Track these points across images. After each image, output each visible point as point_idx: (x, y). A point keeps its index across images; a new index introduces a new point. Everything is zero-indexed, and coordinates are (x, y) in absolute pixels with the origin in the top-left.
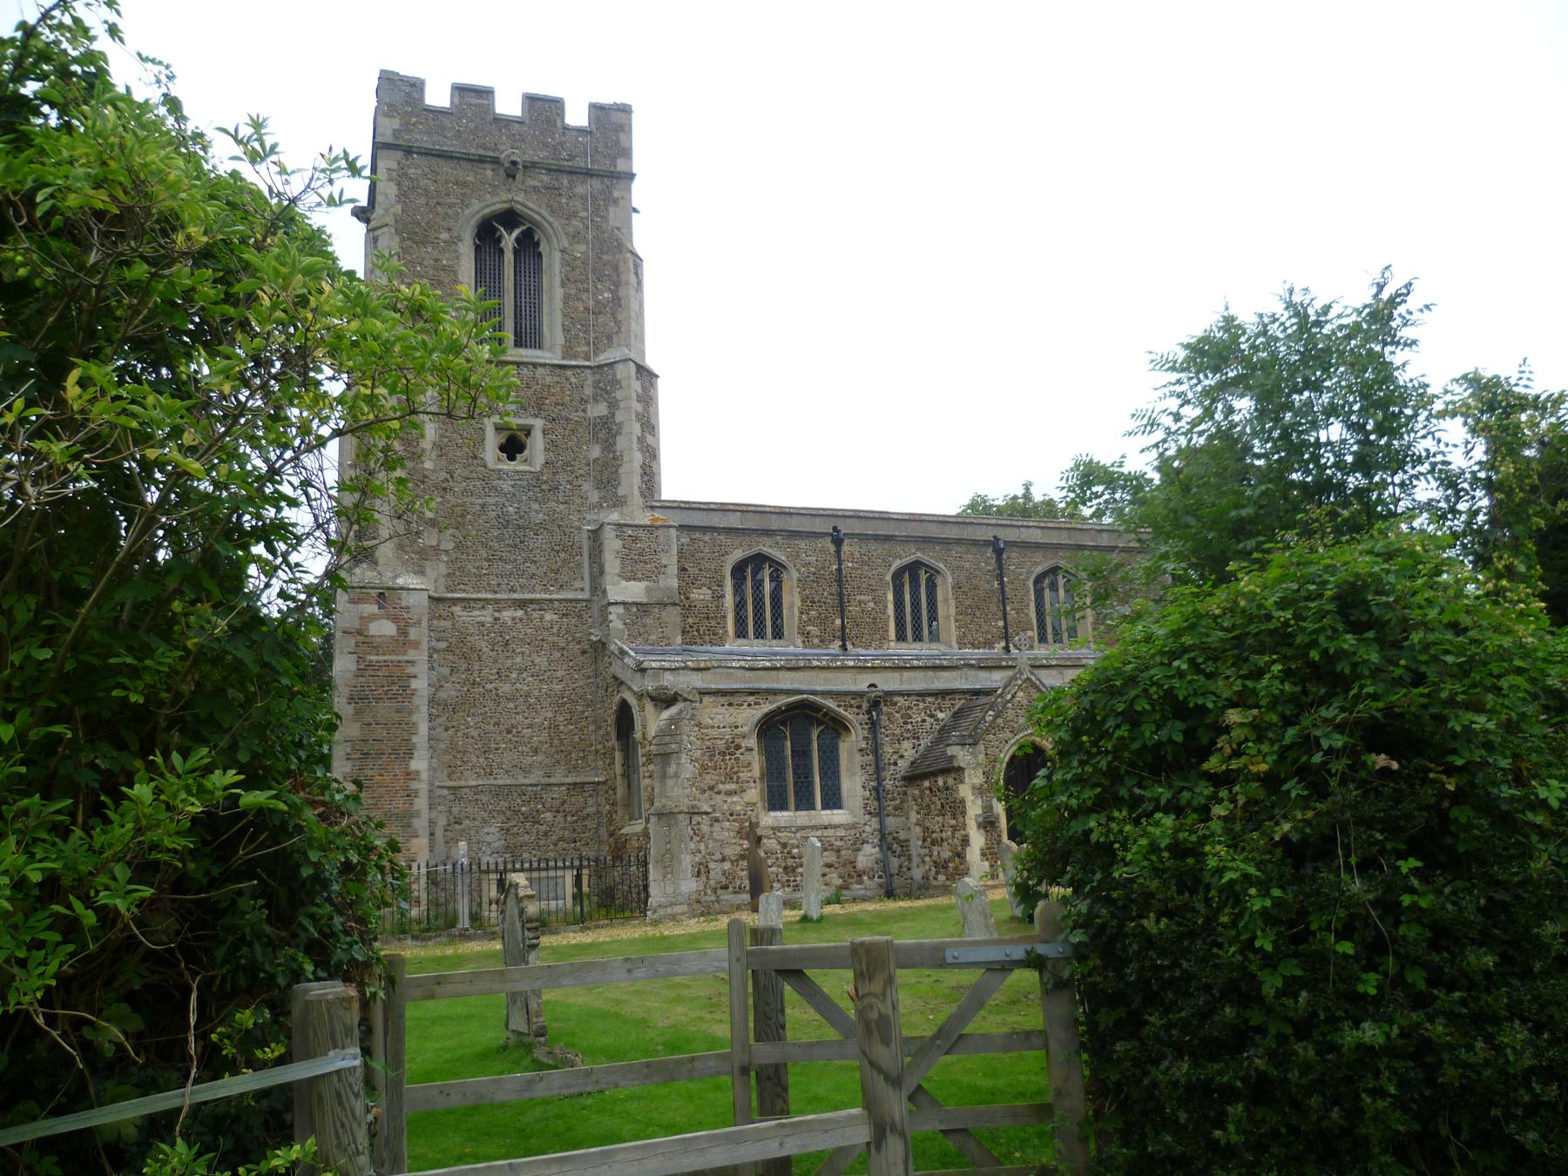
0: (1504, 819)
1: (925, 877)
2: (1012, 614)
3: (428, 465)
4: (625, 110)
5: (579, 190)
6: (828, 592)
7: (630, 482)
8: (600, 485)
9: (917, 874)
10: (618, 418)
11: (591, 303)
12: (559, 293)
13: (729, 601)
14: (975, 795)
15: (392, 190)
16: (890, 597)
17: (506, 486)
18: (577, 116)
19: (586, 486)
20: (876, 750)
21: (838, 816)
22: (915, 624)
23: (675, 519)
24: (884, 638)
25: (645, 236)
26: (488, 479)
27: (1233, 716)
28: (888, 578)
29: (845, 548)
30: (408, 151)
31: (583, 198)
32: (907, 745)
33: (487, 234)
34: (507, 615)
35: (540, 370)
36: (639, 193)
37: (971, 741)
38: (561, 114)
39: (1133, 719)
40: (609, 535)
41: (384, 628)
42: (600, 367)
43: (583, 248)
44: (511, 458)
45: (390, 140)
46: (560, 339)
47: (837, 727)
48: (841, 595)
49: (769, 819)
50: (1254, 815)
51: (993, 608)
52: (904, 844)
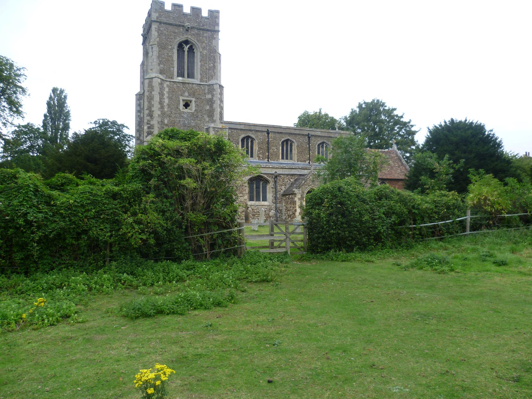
0: (350, 212)
1: (286, 219)
2: (311, 154)
3: (166, 110)
4: (218, 12)
5: (205, 35)
6: (265, 146)
7: (217, 116)
8: (209, 116)
9: (284, 218)
10: (214, 99)
11: (208, 67)
12: (199, 64)
14: (299, 201)
16: (281, 148)
17: (185, 116)
18: (205, 14)
19: (205, 116)
20: (276, 188)
21: (266, 203)
22: (286, 155)
23: (228, 126)
24: (279, 158)
25: (222, 49)
26: (181, 113)
27: (326, 200)
28: (280, 143)
29: (270, 135)
30: (160, 23)
31: (206, 37)
32: (283, 187)
33: (180, 46)
35: (194, 85)
36: (221, 35)
37: (299, 187)
38: (201, 13)
39: (316, 199)
40: (211, 130)
42: (210, 85)
43: (206, 51)
44: (186, 108)
45: (156, 20)
46: (199, 77)
47: (266, 182)
48: (268, 147)
49: (250, 203)
50: (327, 210)
51: (307, 152)
52: (281, 210)
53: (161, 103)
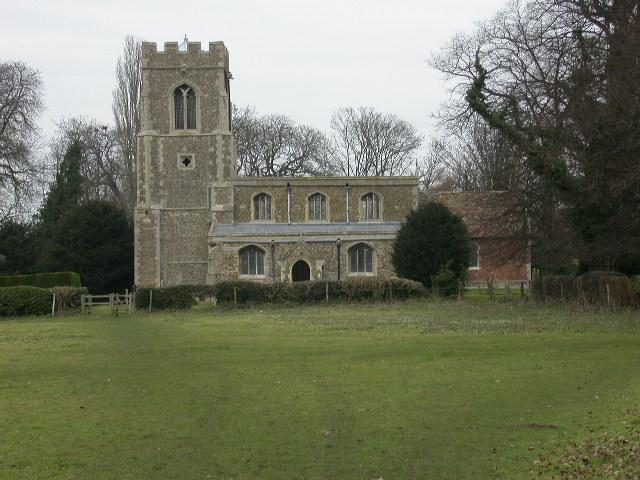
8: (212, 173)
13: (252, 208)
15: (147, 82)
18: (205, 48)
30: (152, 69)
33: (178, 92)
34: (184, 214)
40: (213, 190)
41: (147, 220)
53: (154, 163)
